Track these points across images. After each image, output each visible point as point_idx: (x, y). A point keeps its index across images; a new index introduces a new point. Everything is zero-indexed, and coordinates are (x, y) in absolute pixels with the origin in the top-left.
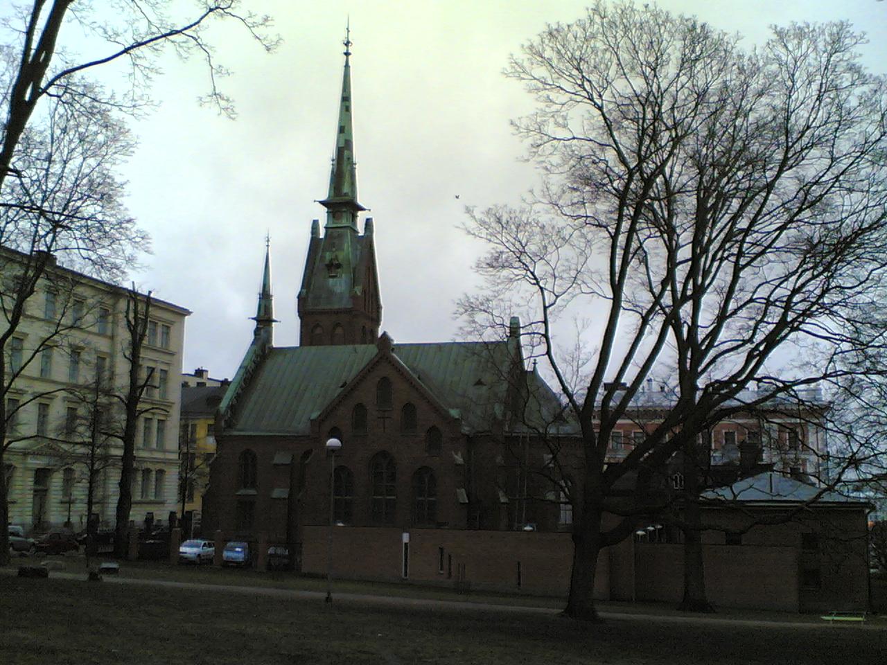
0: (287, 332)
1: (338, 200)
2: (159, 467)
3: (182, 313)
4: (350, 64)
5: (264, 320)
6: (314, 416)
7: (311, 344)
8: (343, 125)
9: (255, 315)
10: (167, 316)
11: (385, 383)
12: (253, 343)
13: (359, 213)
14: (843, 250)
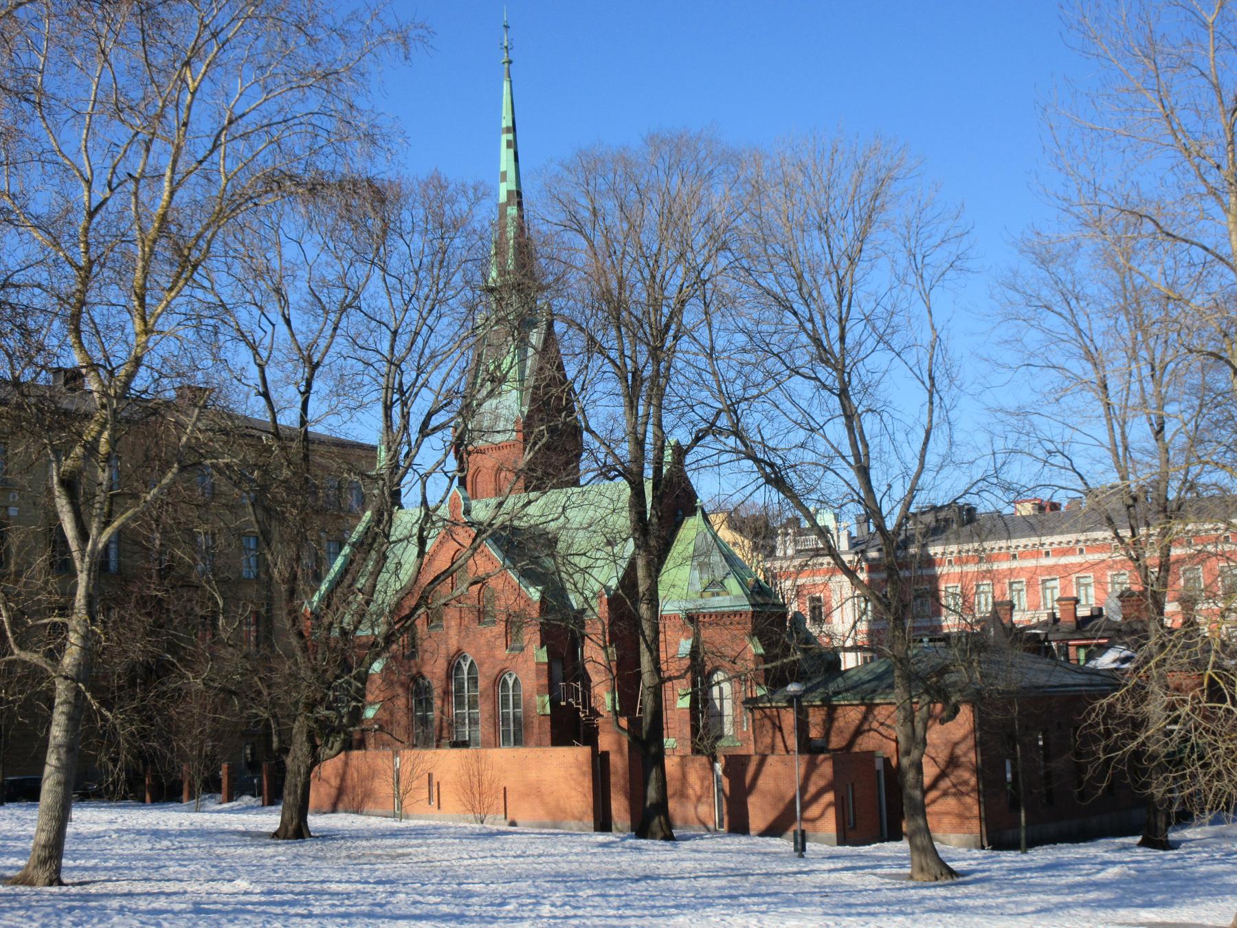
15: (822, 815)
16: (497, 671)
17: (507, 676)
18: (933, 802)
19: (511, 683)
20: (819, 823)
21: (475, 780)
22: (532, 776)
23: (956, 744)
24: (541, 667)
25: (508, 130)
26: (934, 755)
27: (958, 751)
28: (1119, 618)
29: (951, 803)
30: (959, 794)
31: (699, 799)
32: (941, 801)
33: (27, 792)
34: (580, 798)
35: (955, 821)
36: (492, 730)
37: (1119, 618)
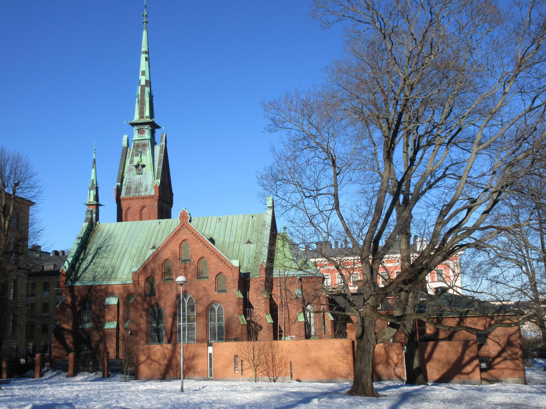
15: (473, 370)
16: (209, 303)
17: (214, 305)
18: (499, 363)
19: (216, 309)
20: (471, 375)
21: (270, 359)
22: (313, 354)
23: (511, 335)
24: (240, 300)
25: (146, 52)
26: (498, 341)
27: (512, 339)
28: (106, 328)
29: (509, 363)
30: (513, 359)
31: (396, 365)
32: (502, 363)
33: (180, 379)
34: (345, 366)
35: (510, 372)
36: (205, 333)
37: (106, 328)
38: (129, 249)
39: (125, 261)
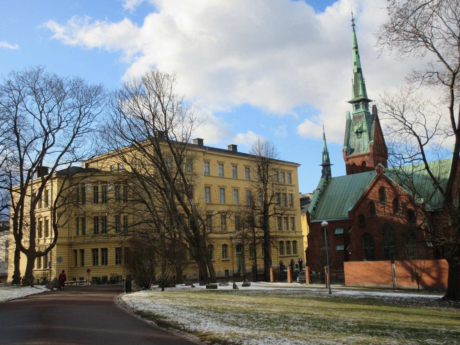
0: (339, 170)
1: (357, 99)
2: (293, 240)
3: (296, 165)
4: (353, 33)
5: (326, 166)
6: (350, 209)
7: (352, 173)
8: (59, 256)
9: (321, 163)
10: (291, 169)
11: (382, 190)
12: (322, 177)
13: (370, 103)
14: (95, 221)
38: (350, 195)
39: (347, 203)
